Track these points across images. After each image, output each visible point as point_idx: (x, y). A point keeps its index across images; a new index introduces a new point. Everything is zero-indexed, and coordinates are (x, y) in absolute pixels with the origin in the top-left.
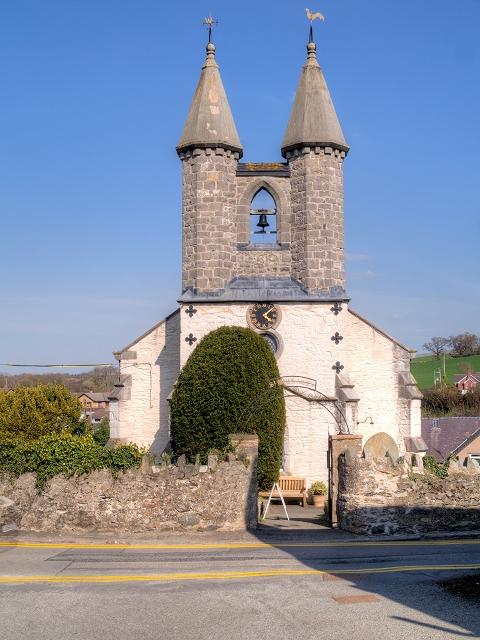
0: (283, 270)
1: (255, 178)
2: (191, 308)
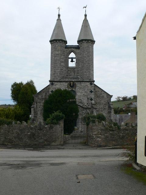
0: (77, 73)
1: (70, 49)
2: (91, 83)
